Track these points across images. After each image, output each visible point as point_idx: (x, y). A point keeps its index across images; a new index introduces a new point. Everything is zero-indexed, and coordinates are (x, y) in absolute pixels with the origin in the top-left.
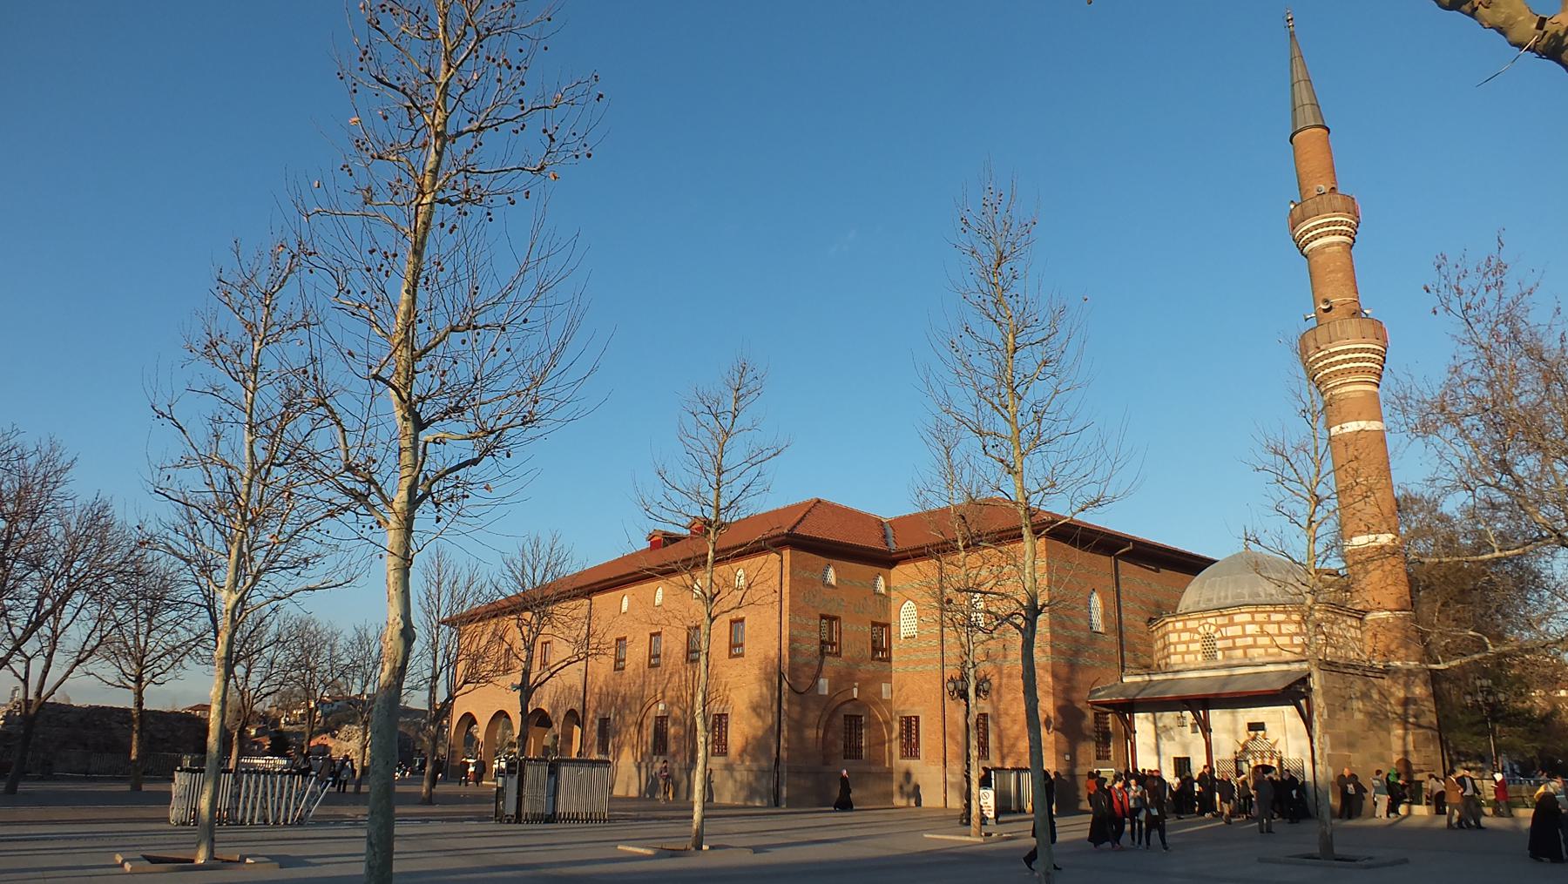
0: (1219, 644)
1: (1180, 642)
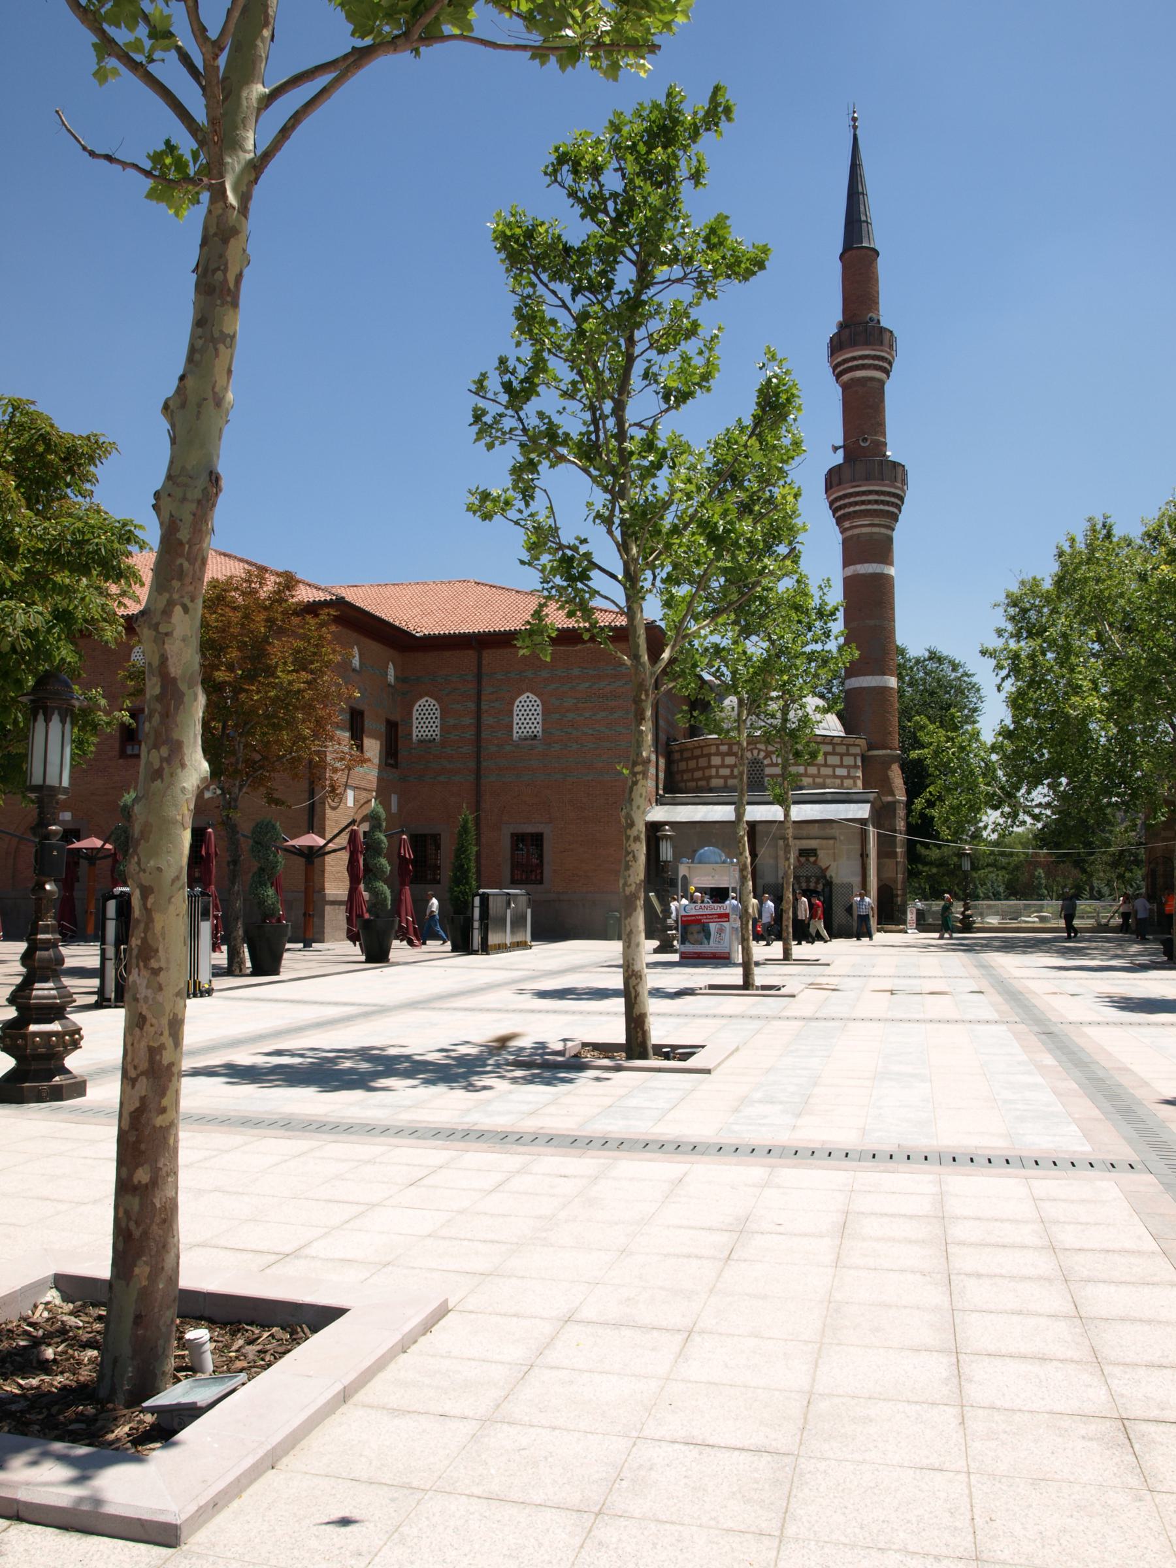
0: (768, 771)
1: (723, 766)
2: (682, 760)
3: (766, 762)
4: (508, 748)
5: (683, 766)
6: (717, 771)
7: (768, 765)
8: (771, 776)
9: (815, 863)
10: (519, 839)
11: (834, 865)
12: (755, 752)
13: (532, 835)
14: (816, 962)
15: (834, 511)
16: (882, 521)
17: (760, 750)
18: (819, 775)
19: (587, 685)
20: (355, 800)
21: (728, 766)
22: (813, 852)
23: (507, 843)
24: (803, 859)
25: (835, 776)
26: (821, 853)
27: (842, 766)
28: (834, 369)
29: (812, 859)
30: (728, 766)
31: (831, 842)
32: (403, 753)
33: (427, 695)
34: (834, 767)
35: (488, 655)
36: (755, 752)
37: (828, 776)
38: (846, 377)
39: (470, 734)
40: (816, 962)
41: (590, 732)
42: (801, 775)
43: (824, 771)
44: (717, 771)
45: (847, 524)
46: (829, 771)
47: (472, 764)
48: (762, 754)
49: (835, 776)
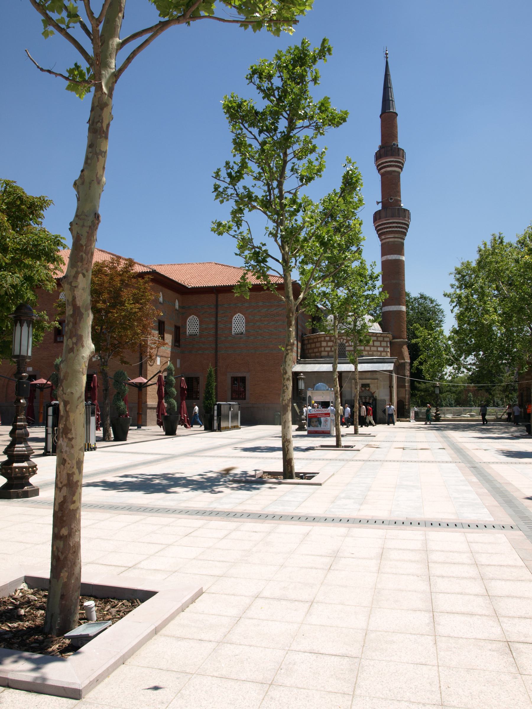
0: (347, 348)
1: (327, 346)
2: (308, 343)
3: (346, 345)
4: (230, 338)
5: (309, 346)
6: (324, 349)
7: (347, 346)
8: (349, 351)
9: (369, 390)
10: (235, 379)
11: (377, 391)
12: (342, 340)
13: (241, 377)
14: (369, 435)
15: (378, 231)
16: (399, 236)
17: (344, 339)
18: (370, 351)
19: (266, 310)
20: (161, 362)
21: (329, 347)
22: (368, 385)
23: (229, 381)
24: (363, 389)
25: (378, 351)
26: (371, 386)
27: (381, 346)
28: (377, 167)
29: (367, 388)
30: (329, 347)
31: (376, 381)
32: (182, 340)
33: (193, 314)
34: (377, 347)
35: (221, 296)
36: (342, 340)
37: (374, 351)
38: (383, 171)
39: (212, 332)
40: (369, 435)
41: (267, 331)
42: (362, 350)
43: (373, 349)
44: (324, 349)
45: (383, 237)
46: (375, 349)
47: (214, 346)
48: (345, 341)
49: (378, 351)
